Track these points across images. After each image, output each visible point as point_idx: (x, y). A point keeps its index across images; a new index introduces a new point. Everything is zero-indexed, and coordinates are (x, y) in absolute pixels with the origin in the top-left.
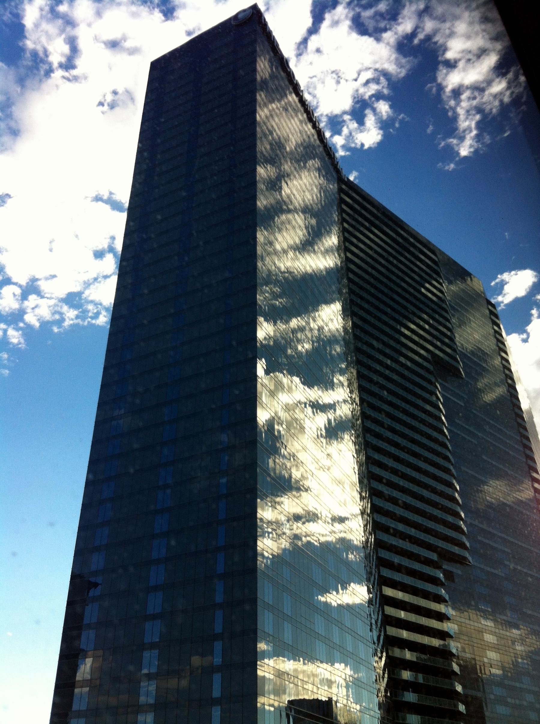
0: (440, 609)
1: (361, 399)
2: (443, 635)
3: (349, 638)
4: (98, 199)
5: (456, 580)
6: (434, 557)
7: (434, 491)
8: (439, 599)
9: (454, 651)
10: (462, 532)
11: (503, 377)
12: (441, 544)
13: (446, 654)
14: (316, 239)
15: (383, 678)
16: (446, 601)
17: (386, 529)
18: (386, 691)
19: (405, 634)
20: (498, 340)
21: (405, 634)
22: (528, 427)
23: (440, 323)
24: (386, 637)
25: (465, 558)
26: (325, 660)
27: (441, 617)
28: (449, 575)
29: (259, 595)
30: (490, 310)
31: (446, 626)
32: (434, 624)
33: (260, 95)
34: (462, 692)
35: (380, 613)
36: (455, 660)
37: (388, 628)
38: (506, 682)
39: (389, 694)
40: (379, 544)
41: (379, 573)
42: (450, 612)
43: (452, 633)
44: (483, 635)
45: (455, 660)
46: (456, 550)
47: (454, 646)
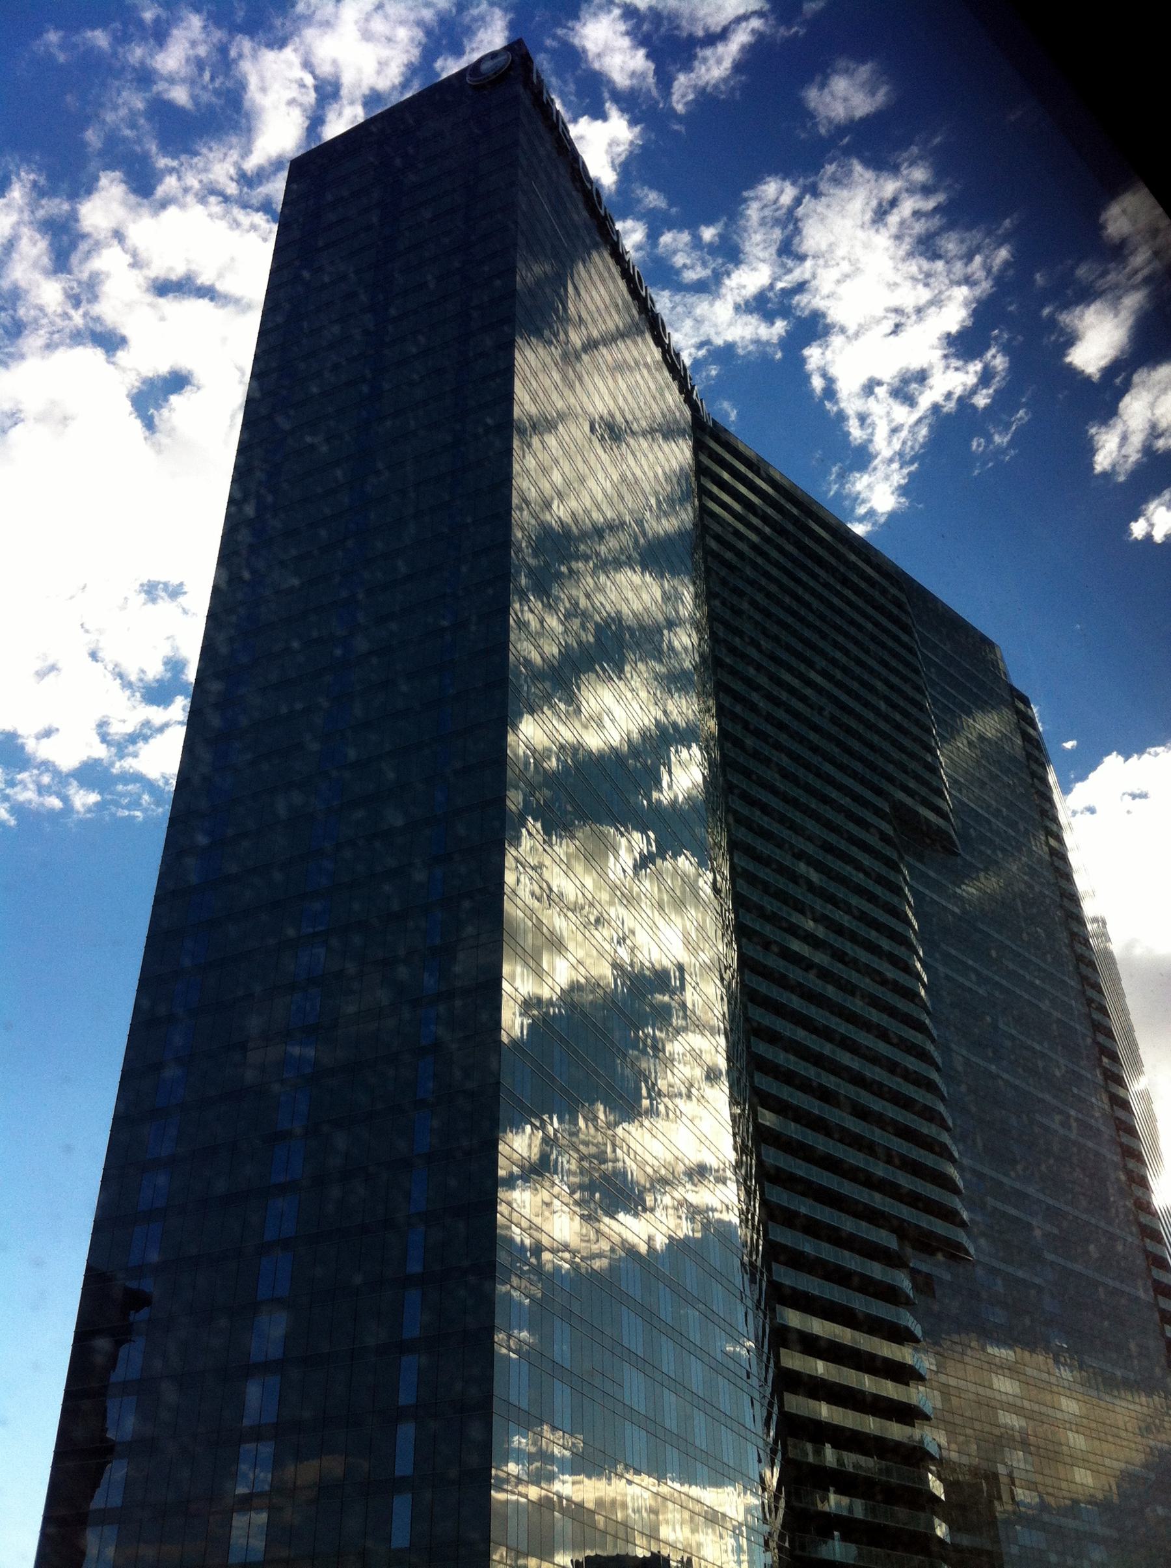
0: (904, 1357)
1: (732, 869)
2: (908, 1414)
3: (700, 1420)
4: (233, 259)
5: (938, 1293)
6: (889, 1241)
7: (874, 949)
8: (900, 1335)
9: (933, 1449)
10: (956, 1191)
11: (1140, 1261)
12: (905, 1212)
13: (916, 1457)
14: (631, 23)
15: (777, 1509)
16: (917, 1341)
17: (788, 1218)
18: (781, 1537)
19: (825, 1411)
20: (1090, 1001)
21: (825, 1411)
22: (1122, 1053)
23: (912, 756)
24: (783, 1414)
25: (959, 1247)
26: (644, 1468)
27: (903, 1374)
28: (925, 1284)
29: (498, 1390)
30: (1051, 848)
31: (916, 1395)
32: (889, 1389)
33: (525, 357)
34: (948, 1540)
35: (772, 1365)
36: (933, 1468)
37: (788, 1397)
38: (1046, 1517)
39: (787, 1545)
40: (774, 1252)
41: (781, 1406)
42: (926, 1363)
43: (928, 1409)
44: (996, 1415)
45: (933, 1468)
46: (940, 1227)
47: (934, 1438)
